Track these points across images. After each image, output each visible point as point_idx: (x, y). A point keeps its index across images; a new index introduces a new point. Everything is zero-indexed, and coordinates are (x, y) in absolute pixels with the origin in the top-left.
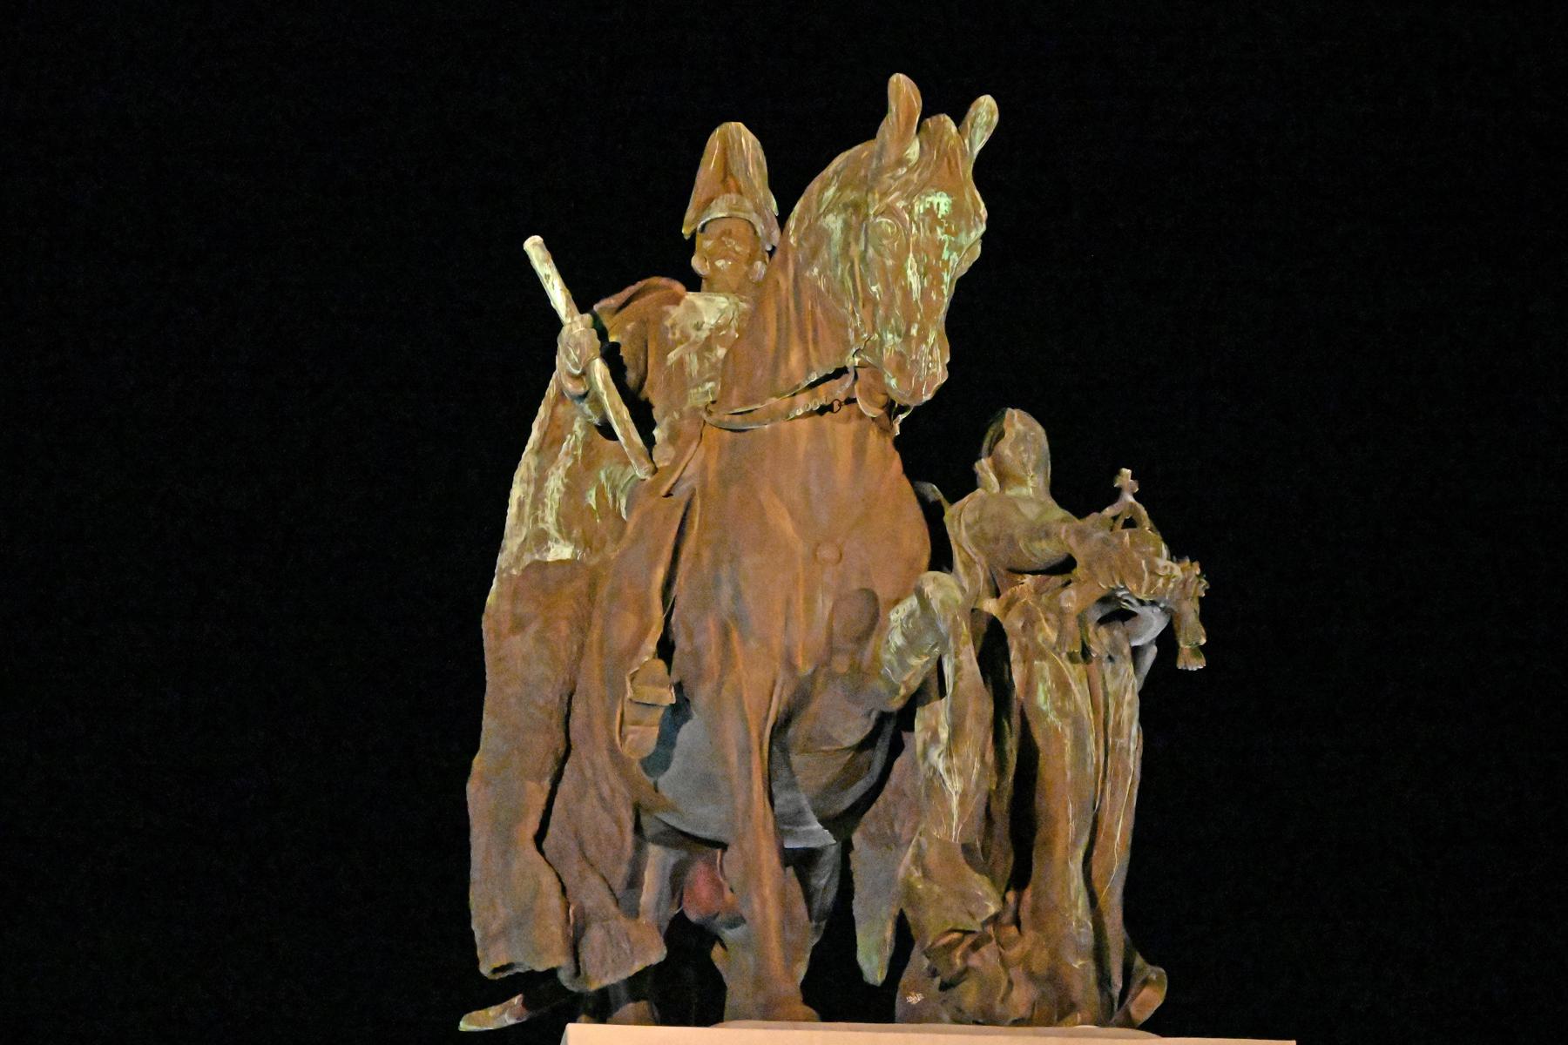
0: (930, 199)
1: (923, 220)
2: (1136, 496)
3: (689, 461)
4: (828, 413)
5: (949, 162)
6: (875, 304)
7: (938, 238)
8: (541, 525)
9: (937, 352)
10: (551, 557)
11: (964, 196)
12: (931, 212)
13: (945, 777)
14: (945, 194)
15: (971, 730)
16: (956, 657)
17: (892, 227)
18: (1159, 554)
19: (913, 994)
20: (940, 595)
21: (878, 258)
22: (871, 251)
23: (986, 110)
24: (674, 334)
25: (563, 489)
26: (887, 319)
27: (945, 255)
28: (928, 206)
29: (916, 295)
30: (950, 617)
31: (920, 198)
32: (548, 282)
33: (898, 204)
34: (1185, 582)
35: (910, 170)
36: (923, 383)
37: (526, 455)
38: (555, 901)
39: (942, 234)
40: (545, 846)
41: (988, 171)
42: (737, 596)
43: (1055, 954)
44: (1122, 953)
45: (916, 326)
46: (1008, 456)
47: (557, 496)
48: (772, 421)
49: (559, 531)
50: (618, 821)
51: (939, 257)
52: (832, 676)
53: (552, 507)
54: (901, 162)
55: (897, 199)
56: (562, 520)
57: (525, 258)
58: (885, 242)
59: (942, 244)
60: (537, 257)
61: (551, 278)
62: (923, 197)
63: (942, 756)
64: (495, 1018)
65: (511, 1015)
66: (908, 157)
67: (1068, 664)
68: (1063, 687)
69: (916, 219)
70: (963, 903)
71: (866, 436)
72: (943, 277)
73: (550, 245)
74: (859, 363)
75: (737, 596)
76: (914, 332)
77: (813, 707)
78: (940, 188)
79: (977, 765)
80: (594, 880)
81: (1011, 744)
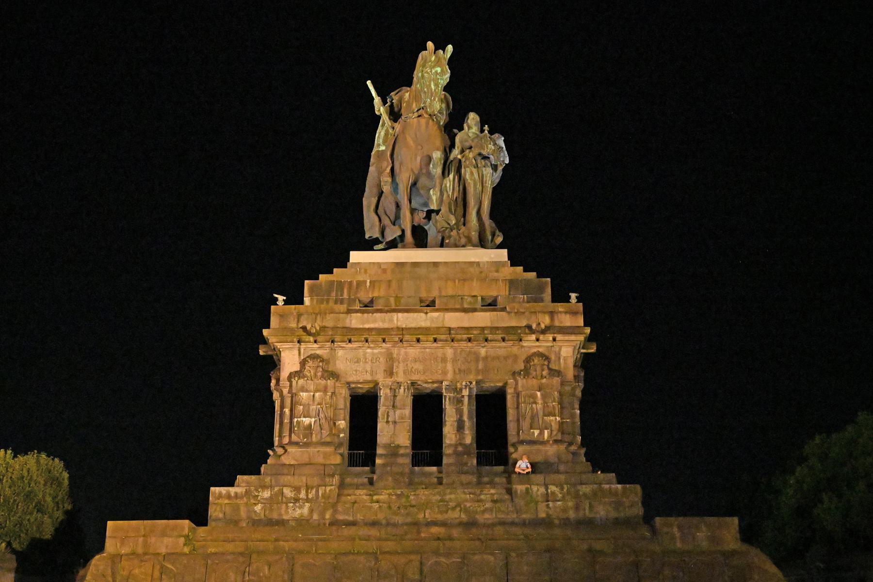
4: (420, 117)
9: (438, 103)
10: (380, 149)
12: (436, 72)
18: (490, 144)
23: (450, 48)
27: (440, 81)
29: (433, 90)
38: (377, 223)
41: (451, 62)
51: (438, 82)
68: (472, 173)
73: (373, 83)
78: (439, 66)
79: (439, 193)
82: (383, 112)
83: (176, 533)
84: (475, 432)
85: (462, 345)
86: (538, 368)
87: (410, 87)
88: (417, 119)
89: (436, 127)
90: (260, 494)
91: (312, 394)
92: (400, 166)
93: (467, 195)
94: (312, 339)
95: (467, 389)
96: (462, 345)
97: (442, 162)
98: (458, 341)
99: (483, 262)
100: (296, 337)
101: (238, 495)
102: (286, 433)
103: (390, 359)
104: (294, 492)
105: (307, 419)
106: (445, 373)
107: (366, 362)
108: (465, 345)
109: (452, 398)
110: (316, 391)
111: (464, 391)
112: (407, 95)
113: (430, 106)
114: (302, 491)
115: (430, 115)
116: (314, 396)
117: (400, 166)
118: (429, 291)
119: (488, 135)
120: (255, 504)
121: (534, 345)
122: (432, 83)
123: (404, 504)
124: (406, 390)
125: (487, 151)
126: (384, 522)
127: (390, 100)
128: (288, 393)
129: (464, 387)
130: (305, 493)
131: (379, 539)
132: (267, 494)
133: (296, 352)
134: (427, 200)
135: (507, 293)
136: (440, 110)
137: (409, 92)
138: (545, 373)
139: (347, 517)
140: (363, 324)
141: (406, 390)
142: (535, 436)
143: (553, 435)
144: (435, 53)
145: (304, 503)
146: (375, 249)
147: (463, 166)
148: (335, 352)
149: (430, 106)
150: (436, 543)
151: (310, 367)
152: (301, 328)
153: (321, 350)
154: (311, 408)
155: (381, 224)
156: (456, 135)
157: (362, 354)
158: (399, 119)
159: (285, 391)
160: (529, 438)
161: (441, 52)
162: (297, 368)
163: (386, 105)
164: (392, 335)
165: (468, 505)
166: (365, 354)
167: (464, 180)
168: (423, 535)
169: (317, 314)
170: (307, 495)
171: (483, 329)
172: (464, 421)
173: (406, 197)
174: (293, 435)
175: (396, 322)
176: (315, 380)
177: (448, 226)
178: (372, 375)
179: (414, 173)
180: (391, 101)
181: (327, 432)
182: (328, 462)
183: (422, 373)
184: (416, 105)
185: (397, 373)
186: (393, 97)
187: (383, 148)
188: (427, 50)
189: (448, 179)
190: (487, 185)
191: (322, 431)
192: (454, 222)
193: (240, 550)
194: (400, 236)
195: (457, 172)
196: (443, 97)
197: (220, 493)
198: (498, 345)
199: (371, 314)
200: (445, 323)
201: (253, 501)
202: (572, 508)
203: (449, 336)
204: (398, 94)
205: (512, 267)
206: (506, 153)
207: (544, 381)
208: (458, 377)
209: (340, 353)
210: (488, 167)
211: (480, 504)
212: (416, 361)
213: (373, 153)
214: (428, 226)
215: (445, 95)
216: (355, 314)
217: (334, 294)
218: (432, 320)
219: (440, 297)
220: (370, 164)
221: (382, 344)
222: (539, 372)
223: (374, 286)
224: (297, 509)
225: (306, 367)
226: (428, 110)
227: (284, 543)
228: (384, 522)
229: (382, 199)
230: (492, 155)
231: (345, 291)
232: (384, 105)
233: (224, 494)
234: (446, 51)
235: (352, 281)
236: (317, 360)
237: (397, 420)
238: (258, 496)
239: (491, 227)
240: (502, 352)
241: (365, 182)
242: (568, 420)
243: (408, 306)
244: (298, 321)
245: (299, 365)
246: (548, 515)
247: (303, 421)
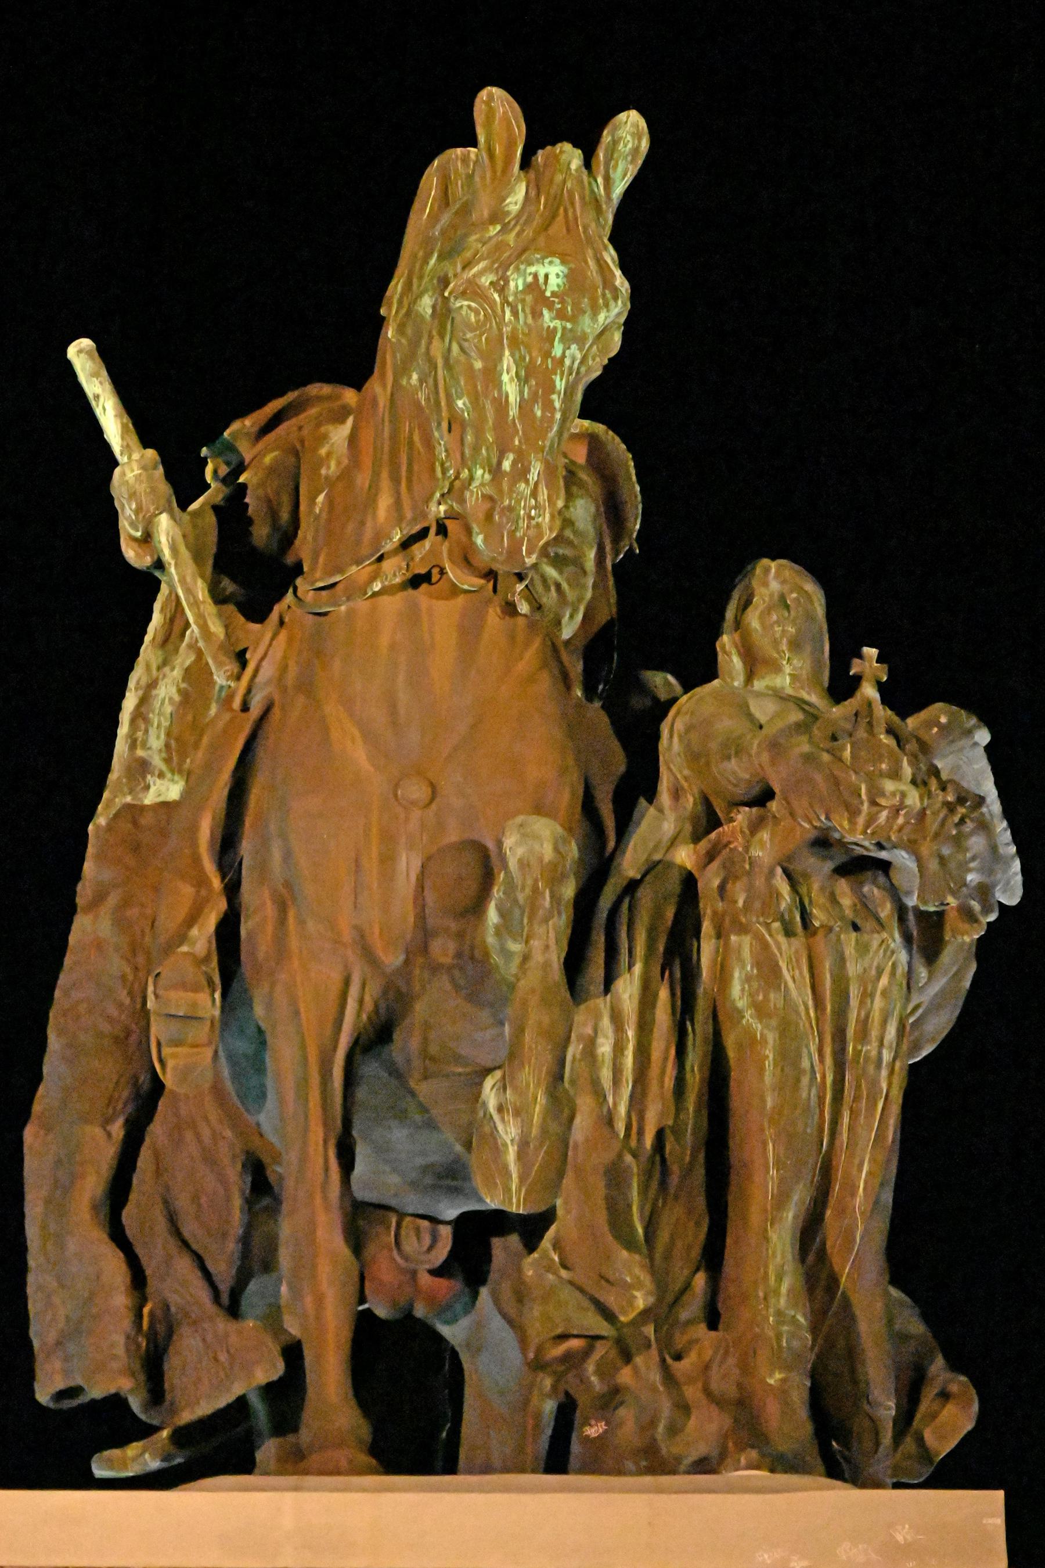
0: (532, 269)
1: (523, 301)
2: (881, 687)
3: (262, 659)
4: (424, 587)
5: (566, 211)
6: (463, 425)
7: (545, 325)
8: (140, 753)
9: (543, 494)
10: (149, 799)
11: (586, 262)
12: (535, 288)
13: (496, 1117)
14: (557, 261)
15: (530, 1048)
16: (527, 942)
17: (477, 313)
19: (593, 1422)
20: (520, 851)
21: (462, 358)
22: (455, 348)
24: (329, 467)
25: (177, 698)
26: (476, 449)
27: (558, 350)
28: (530, 279)
29: (513, 412)
30: (529, 882)
31: (517, 269)
32: (98, 406)
33: (483, 279)
34: (922, 814)
35: (505, 229)
36: (522, 539)
37: (146, 648)
38: (121, 1300)
39: (552, 319)
40: (129, 1215)
42: (288, 856)
43: (746, 1368)
44: (307, 1398)
45: (511, 456)
46: (756, 628)
47: (168, 709)
48: (348, 599)
49: (168, 761)
50: (222, 1180)
51: (547, 354)
52: (435, 969)
53: (159, 726)
54: (496, 216)
55: (481, 273)
56: (173, 743)
57: (68, 368)
58: (469, 335)
59: (552, 333)
60: (83, 369)
61: (102, 400)
62: (522, 267)
63: (495, 1090)
64: (134, 1459)
65: (153, 1457)
66: (506, 209)
67: (782, 939)
69: (511, 299)
70: (195, 1322)
71: (482, 617)
72: (553, 382)
74: (445, 512)
75: (288, 856)
76: (507, 465)
77: (420, 1009)
78: (550, 252)
79: (541, 1099)
80: (184, 1265)
81: (695, 1058)
82: (174, 549)
87: (358, 383)
88: (400, 596)
89: (532, 654)
92: (282, 921)
93: (736, 1125)
97: (569, 890)
112: (340, 434)
113: (489, 517)
115: (491, 575)
117: (282, 921)
119: (882, 713)
122: (507, 360)
125: (871, 819)
127: (224, 470)
134: (458, 1148)
136: (559, 540)
137: (350, 421)
144: (526, 164)
146: (99, 1472)
147: (707, 926)
149: (489, 517)
155: (143, 1300)
156: (662, 708)
158: (280, 596)
161: (571, 155)
163: (194, 506)
173: (317, 1133)
177: (603, 1328)
180: (230, 479)
184: (398, 503)
186: (246, 451)
187: (171, 790)
188: (474, 143)
189: (603, 1004)
192: (641, 1301)
194: (269, 1390)
195: (669, 954)
196: (580, 454)
204: (281, 430)
206: (1002, 828)
210: (881, 925)
213: (102, 818)
214: (465, 1322)
215: (594, 442)
220: (79, 901)
226: (479, 540)
229: (157, 1131)
230: (912, 847)
232: (183, 504)
234: (601, 154)
239: (901, 1338)
241: (23, 1284)
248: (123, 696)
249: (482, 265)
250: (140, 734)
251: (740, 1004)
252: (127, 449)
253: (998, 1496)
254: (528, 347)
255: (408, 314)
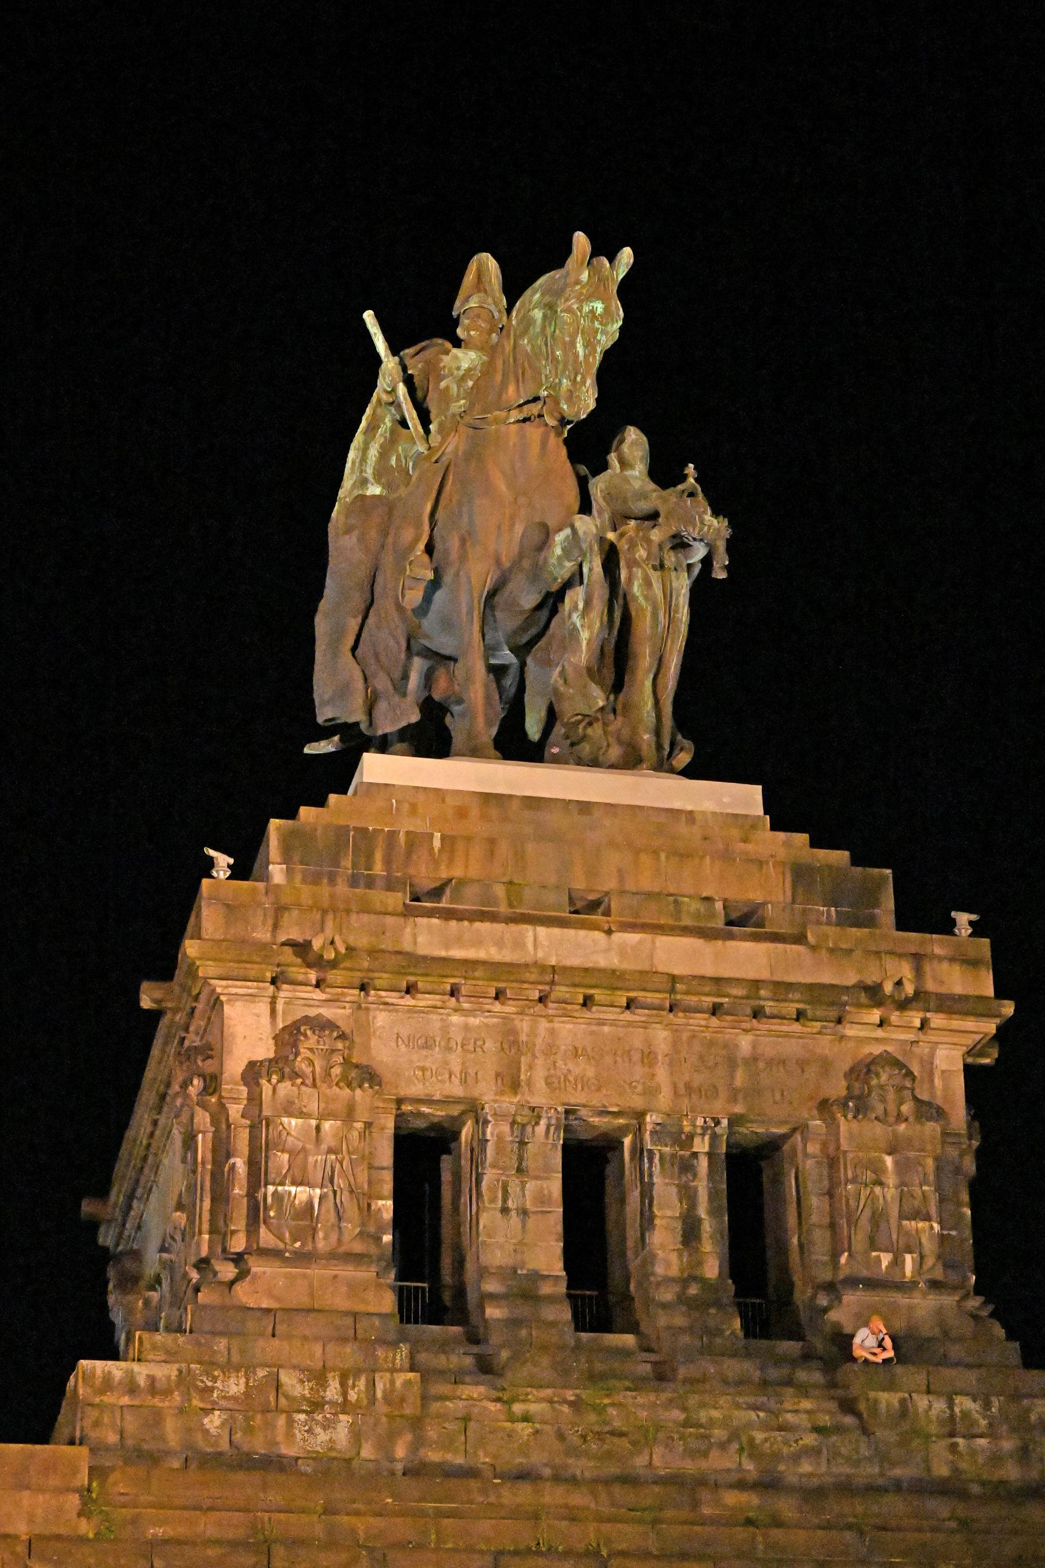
0: (592, 304)
2: (696, 480)
4: (527, 423)
6: (558, 362)
10: (369, 493)
12: (592, 311)
21: (561, 335)
23: (626, 255)
27: (599, 337)
29: (581, 358)
35: (583, 287)
38: (360, 684)
41: (626, 289)
47: (374, 459)
49: (374, 478)
51: (595, 338)
54: (578, 282)
57: (363, 322)
64: (324, 747)
68: (648, 583)
78: (598, 299)
82: (405, 399)
83: (54, 1481)
84: (726, 1250)
85: (696, 1022)
86: (891, 1096)
90: (219, 1384)
91: (314, 1122)
94: (313, 976)
95: (707, 1138)
96: (696, 1022)
98: (688, 1010)
99: (703, 813)
100: (270, 967)
101: (158, 1385)
102: (239, 1222)
103: (510, 1040)
104: (311, 1384)
105: (300, 1189)
106: (651, 1092)
107: (449, 1049)
108: (703, 1023)
109: (668, 1158)
110: (322, 1117)
111: (697, 1140)
114: (330, 1382)
116: (318, 1128)
118: (592, 873)
120: (207, 1412)
121: (873, 1035)
122: (579, 339)
123: (597, 1428)
124: (552, 1129)
126: (547, 1472)
128: (243, 1116)
129: (699, 1131)
130: (338, 1386)
131: (601, 1519)
132: (235, 1386)
133: (264, 1008)
135: (789, 899)
138: (905, 1108)
139: (449, 1457)
140: (447, 947)
141: (552, 1129)
142: (884, 1267)
143: (925, 1268)
145: (335, 1414)
147: (622, 564)
148: (367, 1015)
150: (741, 1534)
151: (311, 1050)
152: (283, 944)
153: (329, 1007)
154: (311, 1159)
157: (438, 1024)
159: (235, 1111)
160: (865, 1273)
162: (265, 1051)
164: (525, 982)
165: (759, 1436)
166: (445, 1028)
167: (625, 596)
168: (706, 1511)
169: (324, 912)
170: (345, 1394)
171: (756, 984)
172: (700, 1220)
174: (263, 1230)
175: (530, 946)
176: (324, 1088)
178: (464, 1082)
179: (498, 562)
181: (354, 1228)
182: (361, 1308)
183: (593, 1088)
185: (529, 1083)
190: (679, 615)
191: (343, 1224)
193: (241, 1533)
197: (107, 1378)
198: (785, 1028)
199: (466, 923)
200: (655, 962)
201: (196, 1402)
202: (1011, 1457)
203: (668, 995)
205: (781, 835)
207: (902, 1127)
208: (685, 1104)
209: (381, 1019)
211: (790, 1436)
212: (576, 1055)
216: (425, 920)
217: (347, 862)
218: (622, 953)
219: (622, 892)
221: (492, 1004)
222: (892, 1107)
223: (452, 852)
224: (318, 1430)
225: (302, 1050)
227: (353, 1520)
228: (547, 1472)
231: (378, 856)
233: (117, 1379)
235: (394, 831)
236: (330, 1034)
237: (529, 1205)
238: (211, 1390)
240: (792, 1048)
242: (954, 1233)
243: (540, 910)
244: (276, 927)
245: (271, 1042)
246: (956, 1470)
247: (290, 1193)
248: (348, 452)
249: (573, 301)
250: (363, 468)
251: (637, 594)
252: (386, 356)
253: (759, 788)
254: (588, 334)
255: (524, 316)
